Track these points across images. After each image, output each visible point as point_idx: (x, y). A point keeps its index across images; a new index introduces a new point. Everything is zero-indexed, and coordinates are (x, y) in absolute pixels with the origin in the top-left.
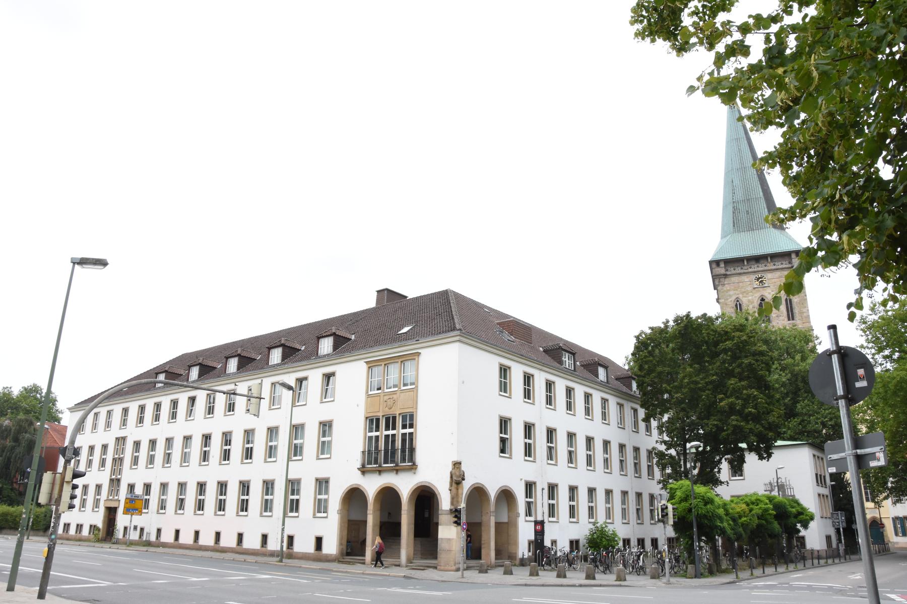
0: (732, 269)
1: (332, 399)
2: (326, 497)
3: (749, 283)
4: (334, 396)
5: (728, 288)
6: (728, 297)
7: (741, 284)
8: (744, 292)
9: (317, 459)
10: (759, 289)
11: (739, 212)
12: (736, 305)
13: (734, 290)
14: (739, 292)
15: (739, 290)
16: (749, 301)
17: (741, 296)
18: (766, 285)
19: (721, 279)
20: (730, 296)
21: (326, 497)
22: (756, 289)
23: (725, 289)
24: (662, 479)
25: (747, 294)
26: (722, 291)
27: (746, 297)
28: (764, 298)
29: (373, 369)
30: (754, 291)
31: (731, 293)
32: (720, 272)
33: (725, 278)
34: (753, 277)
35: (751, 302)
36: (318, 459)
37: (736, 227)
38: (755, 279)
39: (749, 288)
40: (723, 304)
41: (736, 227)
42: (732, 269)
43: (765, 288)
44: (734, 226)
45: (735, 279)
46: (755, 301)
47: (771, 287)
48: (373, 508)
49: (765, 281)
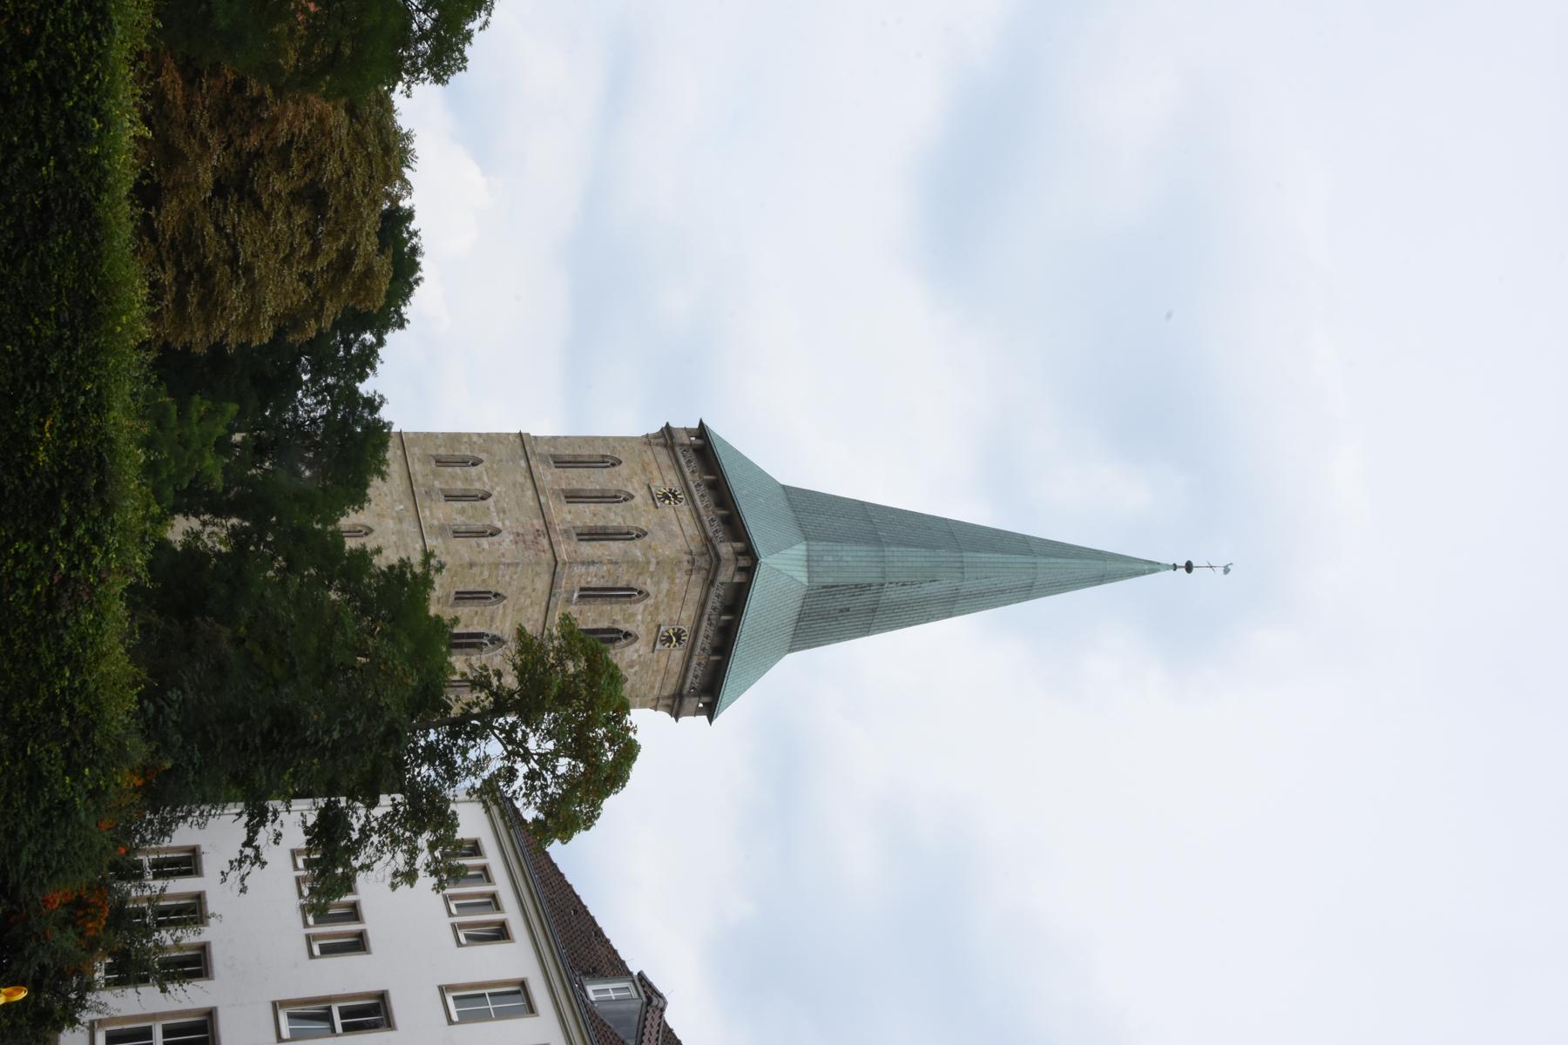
0: (722, 593)
1: (455, 1017)
2: (339, 1028)
3: (676, 618)
4: (464, 1023)
5: (677, 581)
6: (655, 579)
7: (679, 604)
8: (657, 608)
9: (274, 1004)
10: (654, 635)
11: (854, 596)
12: (632, 589)
13: (668, 591)
14: (659, 599)
15: (666, 600)
16: (633, 615)
17: (650, 601)
18: (658, 646)
19: (704, 572)
20: (658, 583)
21: (339, 1028)
22: (655, 630)
23: (679, 575)
24: (373, 834)
25: (651, 614)
26: (676, 569)
27: (644, 610)
28: (630, 639)
29: (519, 996)
30: (652, 625)
31: (665, 586)
32: (723, 573)
33: (705, 580)
34: (686, 627)
35: (630, 617)
36: (277, 1006)
37: (822, 590)
38: (679, 629)
39: (662, 618)
40: (643, 568)
41: (822, 590)
42: (722, 593)
43: (652, 645)
44: (824, 587)
45: (696, 593)
46: (627, 625)
47: (652, 654)
48: (193, 943)
49: (669, 647)
